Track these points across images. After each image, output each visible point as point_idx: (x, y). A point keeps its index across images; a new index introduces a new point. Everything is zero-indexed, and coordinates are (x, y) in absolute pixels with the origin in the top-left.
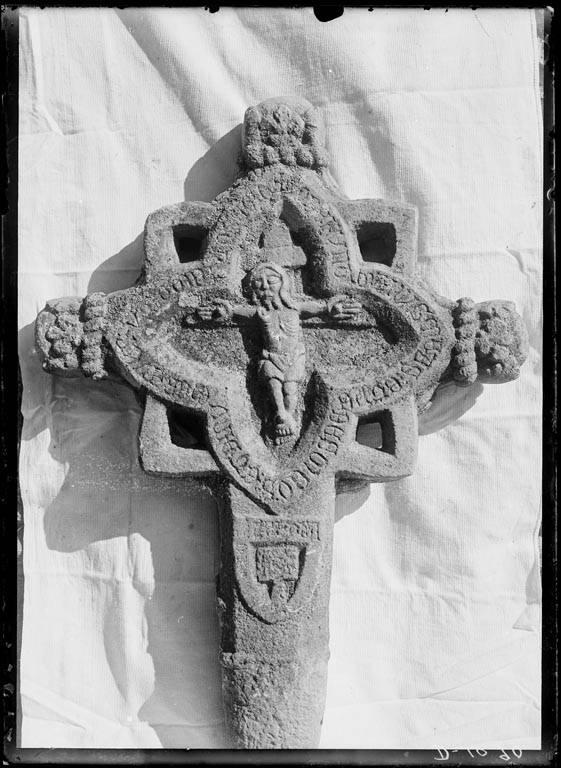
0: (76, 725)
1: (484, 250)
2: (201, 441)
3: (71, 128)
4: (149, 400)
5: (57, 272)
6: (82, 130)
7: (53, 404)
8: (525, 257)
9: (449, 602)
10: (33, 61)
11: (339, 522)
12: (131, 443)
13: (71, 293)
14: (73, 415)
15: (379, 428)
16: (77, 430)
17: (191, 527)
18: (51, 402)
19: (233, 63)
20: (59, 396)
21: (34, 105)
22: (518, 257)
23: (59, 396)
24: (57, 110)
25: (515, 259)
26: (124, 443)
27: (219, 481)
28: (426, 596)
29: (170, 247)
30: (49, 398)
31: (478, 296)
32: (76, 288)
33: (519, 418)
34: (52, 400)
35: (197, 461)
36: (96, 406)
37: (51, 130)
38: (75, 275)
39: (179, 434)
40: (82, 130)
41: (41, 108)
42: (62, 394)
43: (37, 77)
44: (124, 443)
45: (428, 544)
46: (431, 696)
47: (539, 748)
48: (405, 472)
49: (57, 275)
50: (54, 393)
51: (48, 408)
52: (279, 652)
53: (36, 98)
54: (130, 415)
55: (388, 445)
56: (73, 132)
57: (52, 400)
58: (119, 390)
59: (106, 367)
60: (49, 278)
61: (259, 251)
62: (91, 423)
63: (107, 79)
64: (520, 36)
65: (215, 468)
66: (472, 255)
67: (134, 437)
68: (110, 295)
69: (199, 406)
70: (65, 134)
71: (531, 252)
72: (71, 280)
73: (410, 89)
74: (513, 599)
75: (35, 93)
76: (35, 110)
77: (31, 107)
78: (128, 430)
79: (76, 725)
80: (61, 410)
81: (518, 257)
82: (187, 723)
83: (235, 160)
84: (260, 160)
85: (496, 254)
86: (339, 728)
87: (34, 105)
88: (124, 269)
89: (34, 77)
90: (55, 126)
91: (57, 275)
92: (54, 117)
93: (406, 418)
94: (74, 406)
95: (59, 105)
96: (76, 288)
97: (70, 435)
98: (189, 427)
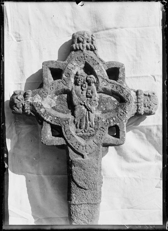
0: (25, 218)
1: (144, 76)
2: (61, 135)
3: (19, 40)
4: (44, 122)
5: (15, 83)
6: (23, 40)
7: (15, 123)
10: (7, 20)
12: (39, 134)
13: (19, 89)
14: (21, 126)
15: (115, 131)
16: (22, 131)
17: (58, 158)
19: (67, 21)
21: (8, 33)
24: (15, 34)
25: (153, 78)
26: (36, 135)
27: (65, 147)
28: (129, 178)
29: (50, 75)
30: (14, 121)
32: (21, 88)
33: (154, 126)
34: (15, 122)
35: (59, 141)
36: (27, 123)
37: (13, 40)
38: (21, 84)
39: (53, 131)
40: (23, 40)
41: (10, 33)
43: (9, 25)
44: (36, 135)
45: (128, 162)
47: (162, 224)
48: (122, 142)
49: (15, 84)
50: (15, 120)
51: (13, 124)
53: (8, 31)
54: (38, 126)
55: (118, 136)
56: (19, 41)
57: (15, 122)
58: (35, 119)
59: (32, 111)
60: (13, 86)
61: (37, 100)
62: (25, 129)
63: (30, 24)
64: (157, 8)
66: (140, 77)
67: (40, 132)
68: (33, 91)
71: (158, 76)
72: (20, 85)
73: (122, 28)
75: (8, 29)
76: (8, 34)
77: (7, 34)
78: (38, 130)
79: (25, 218)
80: (18, 125)
82: (58, 217)
83: (71, 48)
84: (75, 48)
85: (147, 76)
86: (104, 219)
87: (8, 33)
88: (35, 81)
89: (8, 25)
90: (14, 39)
91: (15, 84)
93: (123, 127)
94: (21, 124)
95: (16, 33)
96: (21, 88)
97: (20, 132)
98: (57, 130)
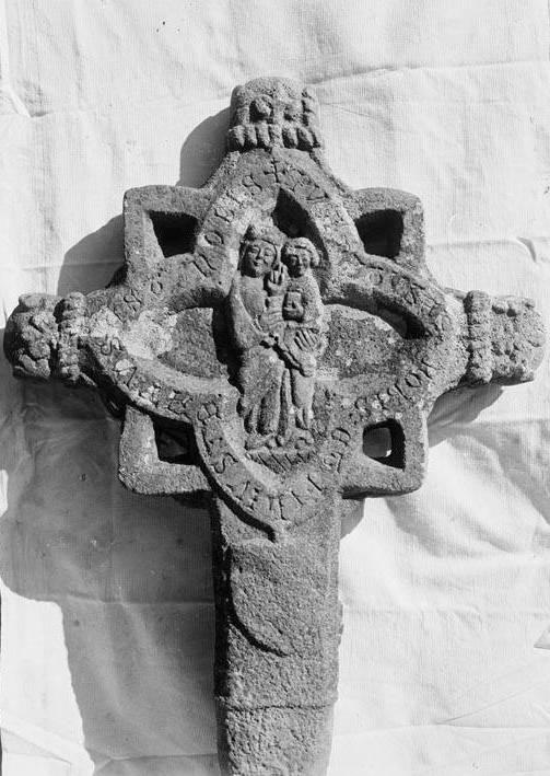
2: (191, 457)
4: (130, 410)
6: (52, 111)
8: (536, 245)
9: (463, 617)
11: (344, 539)
12: (109, 454)
13: (40, 289)
14: (46, 424)
15: (389, 441)
16: (50, 441)
17: (180, 541)
18: (21, 412)
20: (31, 404)
22: (530, 246)
23: (31, 404)
24: (24, 90)
25: (526, 248)
26: (101, 457)
27: (205, 501)
29: (151, 240)
30: (19, 406)
31: (495, 287)
32: (45, 285)
33: (530, 422)
34: (23, 409)
35: (182, 479)
39: (164, 443)
40: (52, 111)
42: (32, 401)
44: (101, 457)
46: (447, 722)
49: (26, 270)
51: (17, 417)
52: (239, 532)
55: (397, 460)
56: (40, 114)
59: (84, 369)
65: (206, 487)
66: (478, 244)
69: (234, 642)
70: (32, 116)
73: (413, 66)
74: (535, 615)
78: (106, 438)
81: (530, 246)
82: (182, 753)
84: (242, 141)
85: (505, 243)
88: (97, 261)
91: (26, 270)
92: (20, 96)
95: (27, 85)
96: (45, 285)
98: (177, 440)
